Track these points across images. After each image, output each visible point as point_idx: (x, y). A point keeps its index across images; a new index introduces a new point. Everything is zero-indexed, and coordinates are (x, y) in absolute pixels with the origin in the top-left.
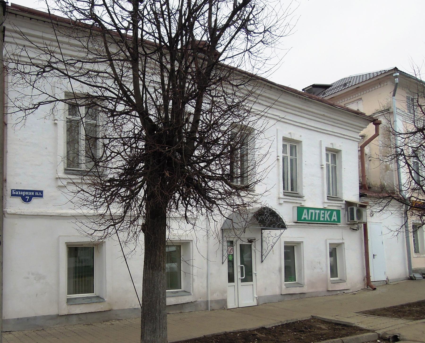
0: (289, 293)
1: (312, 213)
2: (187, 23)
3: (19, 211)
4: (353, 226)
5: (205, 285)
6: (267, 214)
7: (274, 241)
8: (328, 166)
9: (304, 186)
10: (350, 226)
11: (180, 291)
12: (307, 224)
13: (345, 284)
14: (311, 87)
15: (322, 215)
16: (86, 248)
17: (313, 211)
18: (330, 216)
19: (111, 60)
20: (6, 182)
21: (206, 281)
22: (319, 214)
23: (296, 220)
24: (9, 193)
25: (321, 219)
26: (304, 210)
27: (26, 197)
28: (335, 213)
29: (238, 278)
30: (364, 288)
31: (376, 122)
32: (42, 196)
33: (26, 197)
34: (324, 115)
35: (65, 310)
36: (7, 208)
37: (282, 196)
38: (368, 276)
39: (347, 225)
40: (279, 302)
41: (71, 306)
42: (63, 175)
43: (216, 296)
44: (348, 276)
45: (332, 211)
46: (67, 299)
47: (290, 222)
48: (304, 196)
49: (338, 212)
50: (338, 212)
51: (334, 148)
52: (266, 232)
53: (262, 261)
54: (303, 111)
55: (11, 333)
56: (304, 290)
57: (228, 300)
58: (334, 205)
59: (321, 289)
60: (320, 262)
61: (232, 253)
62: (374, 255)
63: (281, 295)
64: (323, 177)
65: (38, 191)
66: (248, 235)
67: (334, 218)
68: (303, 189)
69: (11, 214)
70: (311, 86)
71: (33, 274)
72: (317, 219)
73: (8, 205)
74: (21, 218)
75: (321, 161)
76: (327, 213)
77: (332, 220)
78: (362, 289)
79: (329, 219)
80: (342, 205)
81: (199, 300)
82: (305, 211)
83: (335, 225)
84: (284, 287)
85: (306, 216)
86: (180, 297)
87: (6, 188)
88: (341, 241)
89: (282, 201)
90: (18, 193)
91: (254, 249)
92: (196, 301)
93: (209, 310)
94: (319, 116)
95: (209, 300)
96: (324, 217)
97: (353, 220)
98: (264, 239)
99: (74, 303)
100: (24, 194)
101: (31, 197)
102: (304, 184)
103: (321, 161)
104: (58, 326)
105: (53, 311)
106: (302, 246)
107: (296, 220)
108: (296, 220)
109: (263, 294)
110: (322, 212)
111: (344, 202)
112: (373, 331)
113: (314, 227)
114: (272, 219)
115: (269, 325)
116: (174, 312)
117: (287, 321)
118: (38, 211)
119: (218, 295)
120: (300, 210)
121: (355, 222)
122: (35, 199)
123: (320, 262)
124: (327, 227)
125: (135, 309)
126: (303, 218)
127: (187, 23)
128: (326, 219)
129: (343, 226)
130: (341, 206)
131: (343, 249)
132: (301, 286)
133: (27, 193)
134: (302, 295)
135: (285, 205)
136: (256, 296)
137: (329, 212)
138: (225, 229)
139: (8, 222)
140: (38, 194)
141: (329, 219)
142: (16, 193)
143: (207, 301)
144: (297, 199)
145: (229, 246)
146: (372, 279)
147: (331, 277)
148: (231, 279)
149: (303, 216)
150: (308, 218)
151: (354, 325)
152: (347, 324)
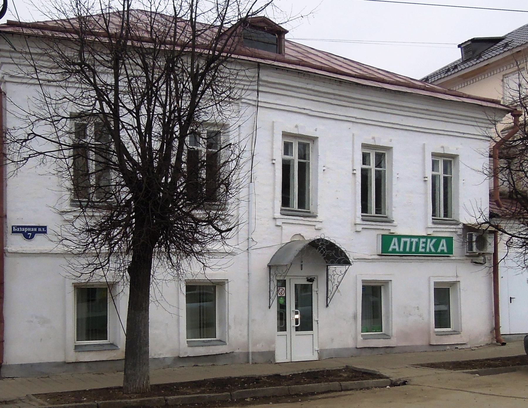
0: (368, 346)
1: (405, 243)
2: (171, 66)
3: (21, 249)
4: (477, 258)
5: (245, 333)
6: (322, 247)
7: (339, 280)
8: (434, 178)
9: (395, 207)
10: (471, 258)
11: (213, 340)
12: (399, 258)
13: (459, 336)
14: (469, 43)
15: (421, 245)
16: (101, 289)
17: (408, 240)
18: (436, 246)
19: (130, 65)
20: (6, 218)
21: (247, 328)
22: (417, 244)
23: (380, 253)
24: (10, 230)
25: (421, 250)
26: (392, 239)
27: (29, 234)
28: (443, 242)
29: (292, 326)
30: (492, 343)
31: (515, 113)
32: (45, 232)
33: (29, 234)
34: (427, 110)
35: (72, 357)
36: (8, 245)
37: (359, 221)
38: (497, 327)
39: (465, 258)
40: (352, 356)
41: (79, 353)
42: (69, 208)
43: (260, 347)
44: (464, 326)
45: (439, 239)
46: (76, 346)
47: (371, 255)
48: (394, 221)
49: (449, 240)
50: (449, 240)
51: (445, 152)
52: (332, 268)
53: (327, 306)
54: (394, 107)
55: (14, 379)
56: (392, 342)
57: (277, 353)
58: (444, 231)
59: (419, 342)
60: (418, 307)
61: (284, 295)
62: (511, 298)
63: (357, 348)
64: (426, 193)
65: (42, 227)
66: (308, 272)
67: (443, 246)
68: (392, 210)
69: (11, 253)
70: (469, 41)
71: (36, 317)
72: (413, 250)
73: (8, 242)
74: (22, 256)
75: (424, 172)
76: (431, 242)
77: (439, 251)
78: (487, 344)
79: (433, 250)
80: (457, 230)
81: (237, 351)
82: (395, 240)
83: (446, 258)
84: (360, 338)
85: (397, 247)
86: (211, 347)
87: (6, 225)
88: (454, 279)
89: (359, 228)
90: (20, 229)
91: (316, 290)
92: (233, 352)
93: (251, 363)
94: (420, 111)
95: (250, 351)
96: (425, 248)
97: (472, 250)
98: (329, 277)
99: (82, 350)
100: (26, 230)
101: (33, 234)
102: (394, 204)
103: (424, 172)
104: (64, 374)
105: (59, 358)
106: (226, 288)
107: (380, 253)
108: (380, 252)
109: (329, 346)
110: (422, 240)
111: (461, 226)
112: (388, 378)
113: (411, 261)
114: (330, 252)
115: (286, 373)
116: (204, 364)
117: (310, 369)
118: (41, 249)
119: (262, 346)
120: (386, 240)
121: (474, 253)
122: (38, 236)
123: (418, 307)
124: (432, 261)
125: (155, 358)
126: (390, 249)
127: (171, 66)
128: (428, 250)
129: (457, 258)
130: (456, 232)
131: (459, 290)
132: (387, 337)
133: (29, 229)
134: (388, 350)
135: (365, 232)
136: (317, 348)
137: (434, 241)
138: (272, 266)
139: (9, 262)
140: (41, 230)
141: (433, 250)
142: (17, 230)
143: (248, 353)
144: (383, 224)
145: (279, 287)
146: (503, 331)
147: (435, 328)
148: (282, 327)
149: (392, 247)
150: (399, 248)
151: (378, 373)
152: (373, 373)
